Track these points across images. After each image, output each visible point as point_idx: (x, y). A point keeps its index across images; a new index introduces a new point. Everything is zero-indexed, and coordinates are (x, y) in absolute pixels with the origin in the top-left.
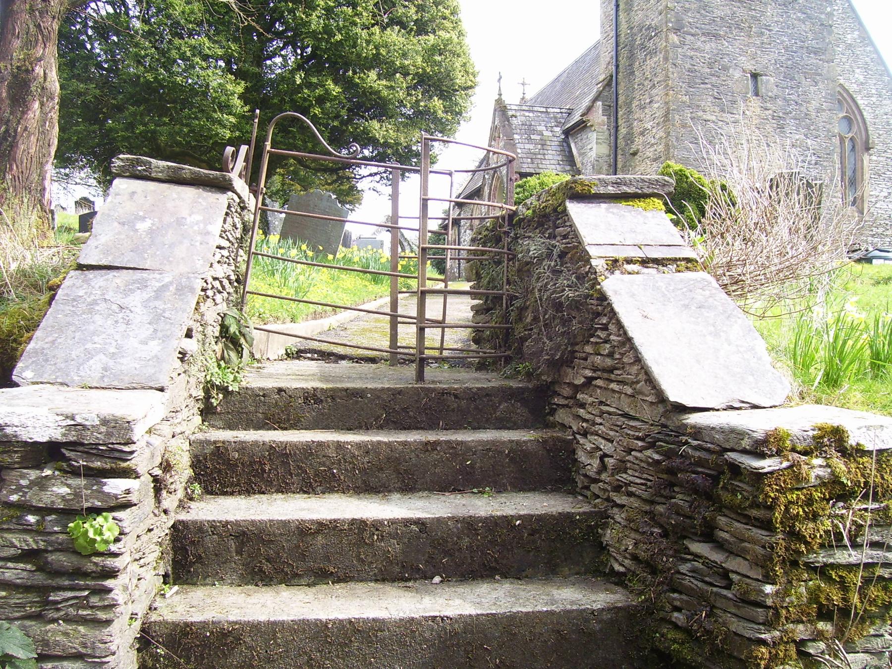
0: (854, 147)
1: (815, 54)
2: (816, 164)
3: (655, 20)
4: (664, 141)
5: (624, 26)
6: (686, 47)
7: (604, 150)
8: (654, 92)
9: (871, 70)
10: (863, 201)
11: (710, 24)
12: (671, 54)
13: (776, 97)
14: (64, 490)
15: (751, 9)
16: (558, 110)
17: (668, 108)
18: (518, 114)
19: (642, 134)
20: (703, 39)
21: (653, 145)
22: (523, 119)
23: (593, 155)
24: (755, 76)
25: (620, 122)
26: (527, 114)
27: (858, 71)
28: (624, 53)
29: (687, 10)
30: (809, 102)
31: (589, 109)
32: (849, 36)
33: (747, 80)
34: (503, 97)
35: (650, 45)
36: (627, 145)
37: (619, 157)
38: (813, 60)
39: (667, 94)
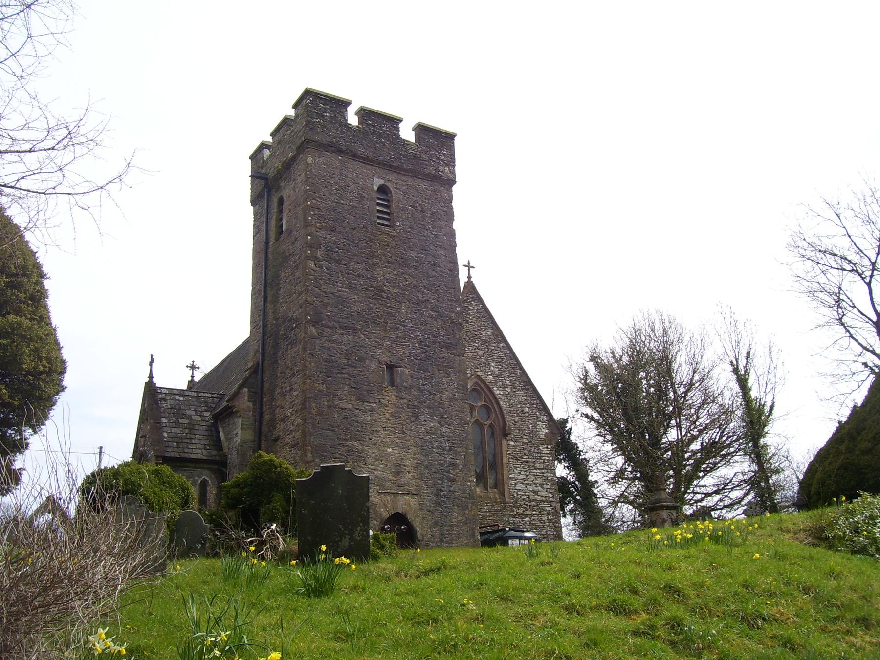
0: (493, 433)
1: (447, 348)
2: (450, 450)
3: (296, 313)
4: (301, 428)
5: (270, 317)
6: (324, 339)
7: (249, 435)
8: (294, 380)
9: (505, 363)
10: (503, 484)
11: (347, 318)
12: (309, 345)
13: (411, 387)
14: (478, 490)
15: (386, 306)
16: (210, 395)
17: (305, 396)
18: (168, 398)
19: (283, 420)
20: (340, 331)
21: (292, 431)
22: (173, 402)
23: (238, 440)
24: (391, 367)
25: (265, 408)
26: (177, 398)
27: (493, 364)
28: (270, 342)
29: (325, 305)
30: (442, 392)
31: (235, 395)
32: (484, 333)
33: (383, 371)
34: (154, 380)
35: (292, 335)
36: (270, 431)
37: (263, 442)
38: (445, 354)
39: (304, 383)
